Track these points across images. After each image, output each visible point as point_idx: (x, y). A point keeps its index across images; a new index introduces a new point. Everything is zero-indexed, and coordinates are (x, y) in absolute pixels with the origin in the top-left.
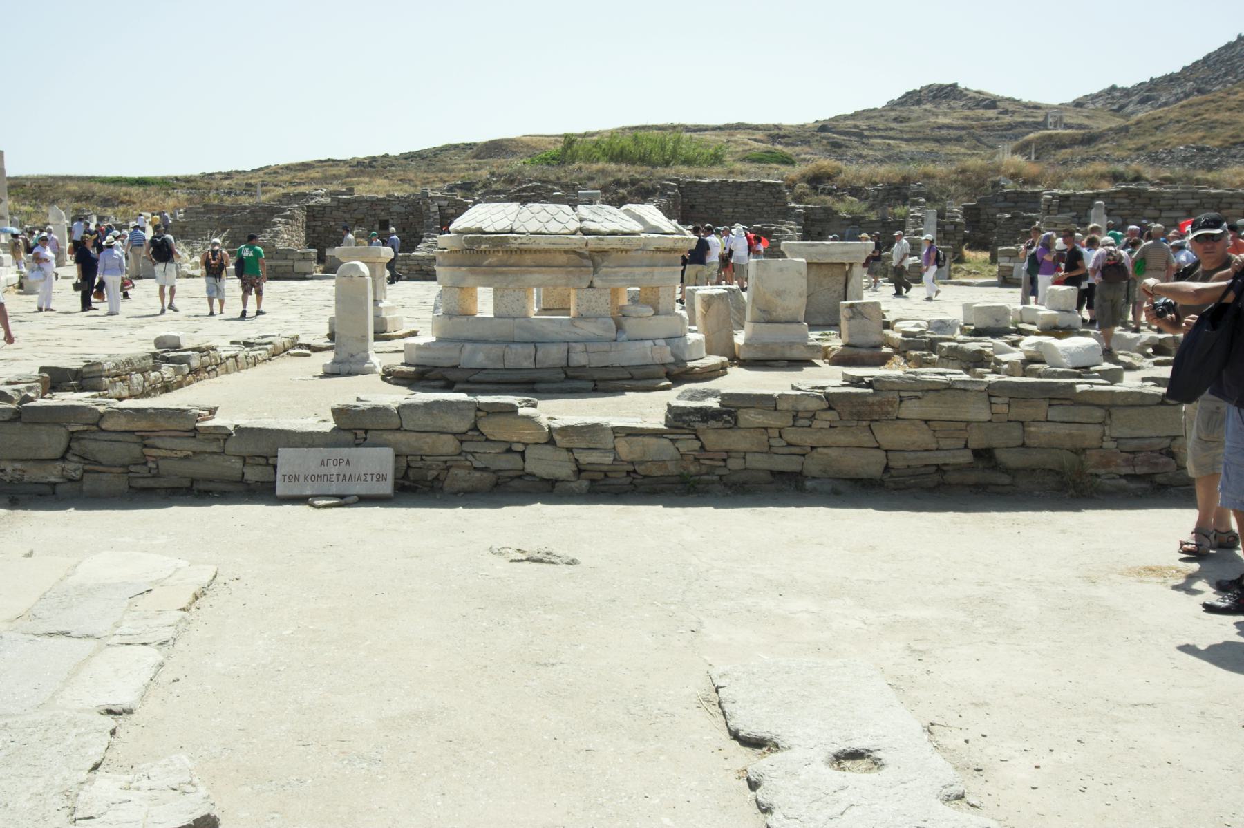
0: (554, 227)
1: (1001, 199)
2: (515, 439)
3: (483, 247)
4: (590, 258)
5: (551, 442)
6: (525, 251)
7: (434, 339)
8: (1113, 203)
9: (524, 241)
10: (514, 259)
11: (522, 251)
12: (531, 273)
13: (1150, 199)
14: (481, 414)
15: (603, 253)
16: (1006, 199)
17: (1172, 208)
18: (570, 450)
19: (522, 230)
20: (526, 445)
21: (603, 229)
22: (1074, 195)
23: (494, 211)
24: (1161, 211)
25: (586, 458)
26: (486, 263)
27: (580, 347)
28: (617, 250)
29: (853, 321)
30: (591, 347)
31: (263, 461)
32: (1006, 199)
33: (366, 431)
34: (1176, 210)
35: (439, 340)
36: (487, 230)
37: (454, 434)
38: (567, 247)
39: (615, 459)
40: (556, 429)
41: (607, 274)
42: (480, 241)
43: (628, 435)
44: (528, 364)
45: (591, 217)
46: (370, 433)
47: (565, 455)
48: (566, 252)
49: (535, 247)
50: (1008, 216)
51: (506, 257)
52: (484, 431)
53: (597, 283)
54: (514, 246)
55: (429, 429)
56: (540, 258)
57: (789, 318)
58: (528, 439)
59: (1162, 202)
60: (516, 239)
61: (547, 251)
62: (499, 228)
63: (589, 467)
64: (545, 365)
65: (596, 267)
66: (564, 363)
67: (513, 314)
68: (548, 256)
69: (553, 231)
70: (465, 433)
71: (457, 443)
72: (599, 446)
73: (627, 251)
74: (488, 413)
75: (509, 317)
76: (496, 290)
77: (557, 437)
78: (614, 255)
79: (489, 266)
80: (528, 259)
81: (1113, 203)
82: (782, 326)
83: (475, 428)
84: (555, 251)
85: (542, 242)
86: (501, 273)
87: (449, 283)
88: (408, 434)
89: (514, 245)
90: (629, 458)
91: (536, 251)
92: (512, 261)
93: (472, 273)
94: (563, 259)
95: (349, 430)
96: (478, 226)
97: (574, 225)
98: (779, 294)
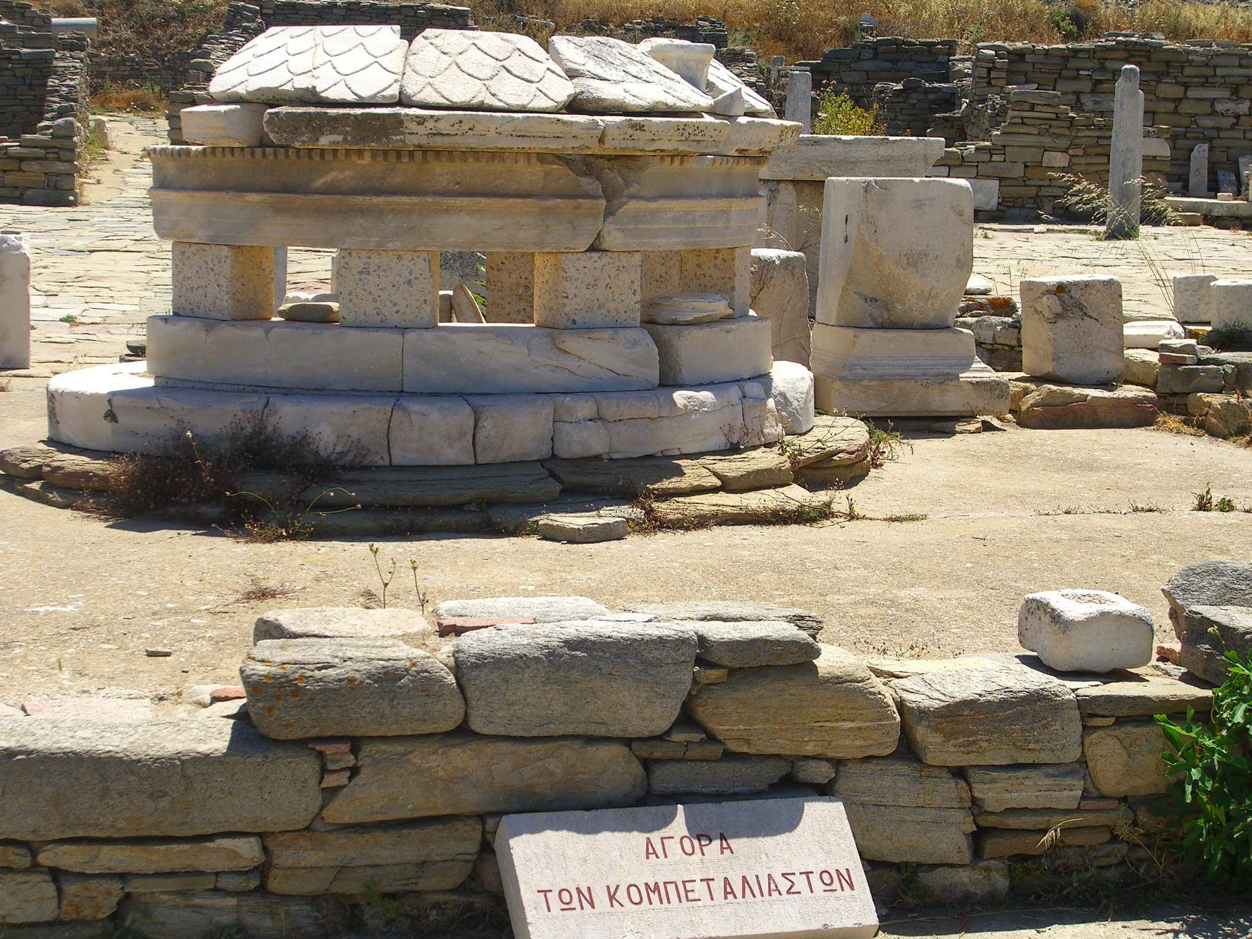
0: (510, 92)
1: (867, 54)
2: (810, 749)
3: (324, 141)
4: (596, 166)
5: (907, 750)
6: (438, 153)
7: (150, 382)
8: (1103, 68)
9: (443, 127)
10: (403, 173)
11: (427, 153)
12: (448, 211)
13: (1168, 63)
14: (714, 674)
15: (626, 161)
16: (876, 56)
17: (1206, 83)
18: (960, 773)
19: (431, 97)
20: (838, 763)
21: (630, 101)
22: (1033, 51)
23: (295, 46)
24: (1186, 86)
25: (997, 794)
26: (320, 183)
27: (584, 408)
28: (662, 155)
29: (1062, 324)
30: (612, 408)
31: (19, 858)
32: (876, 56)
33: (356, 744)
34: (1213, 85)
35: (167, 385)
36: (333, 94)
37: (627, 742)
38: (554, 145)
39: (1085, 796)
40: (923, 713)
41: (637, 217)
42: (317, 125)
43: (1120, 721)
44: (455, 453)
45: (592, 66)
46: (367, 749)
47: (950, 790)
48: (542, 157)
49: (471, 141)
50: (900, 87)
51: (380, 166)
52: (721, 728)
53: (613, 238)
54: (412, 141)
55: (555, 730)
56: (474, 171)
57: (930, 317)
58: (847, 747)
59: (1188, 71)
60: (421, 121)
61: (496, 155)
62: (366, 92)
63: (1012, 822)
64: (503, 456)
65: (611, 194)
66: (545, 451)
67: (395, 319)
68: (497, 166)
69: (515, 101)
70: (662, 737)
71: (637, 769)
72: (1044, 757)
73: (683, 156)
74: (732, 671)
75: (383, 326)
76: (346, 253)
77: (921, 733)
78: (655, 168)
79: (330, 190)
80: (442, 173)
81: (1103, 68)
82: (919, 336)
83: (687, 718)
84: (516, 154)
85: (490, 133)
86: (363, 212)
87: (201, 235)
88: (489, 749)
89: (416, 137)
90: (1123, 789)
91: (476, 154)
92: (397, 179)
93: (279, 210)
94: (531, 174)
95: (302, 744)
96: (302, 83)
97: (562, 90)
98: (913, 260)
